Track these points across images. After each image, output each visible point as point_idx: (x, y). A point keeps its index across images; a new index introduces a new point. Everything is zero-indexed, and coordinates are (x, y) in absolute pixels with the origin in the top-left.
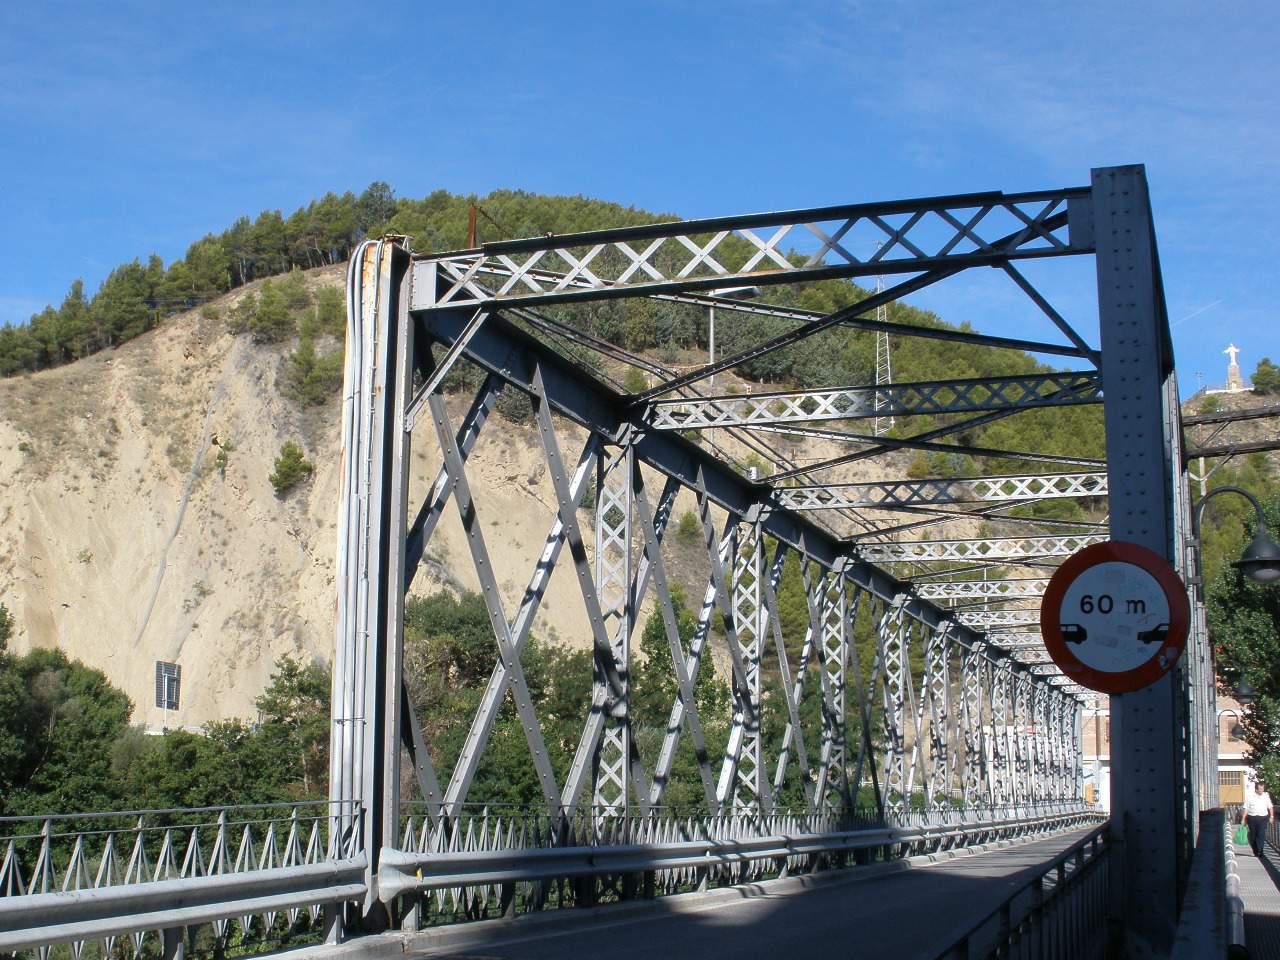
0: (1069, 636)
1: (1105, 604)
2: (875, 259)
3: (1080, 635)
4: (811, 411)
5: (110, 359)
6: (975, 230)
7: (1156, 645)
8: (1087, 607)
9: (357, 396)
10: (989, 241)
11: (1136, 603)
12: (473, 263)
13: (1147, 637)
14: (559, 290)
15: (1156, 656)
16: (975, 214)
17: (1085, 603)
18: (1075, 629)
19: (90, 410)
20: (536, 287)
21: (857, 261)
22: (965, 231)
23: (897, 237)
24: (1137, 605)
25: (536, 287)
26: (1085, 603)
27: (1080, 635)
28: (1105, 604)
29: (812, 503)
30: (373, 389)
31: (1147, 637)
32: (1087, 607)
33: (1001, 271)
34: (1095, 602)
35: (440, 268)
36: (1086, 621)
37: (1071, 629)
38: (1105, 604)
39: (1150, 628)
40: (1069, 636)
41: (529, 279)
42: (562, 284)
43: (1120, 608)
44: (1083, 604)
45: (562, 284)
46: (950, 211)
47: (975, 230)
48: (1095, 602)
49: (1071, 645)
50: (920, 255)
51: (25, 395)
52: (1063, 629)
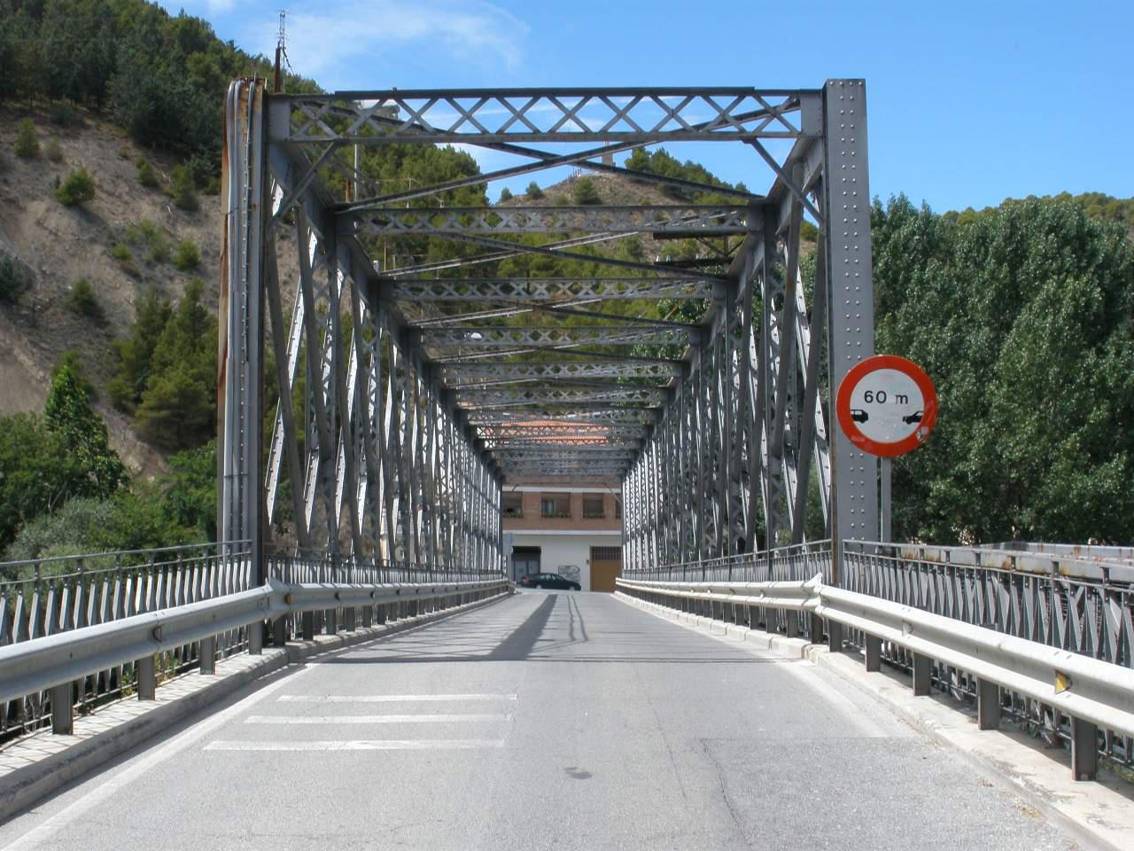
0: (856, 418)
1: (881, 397)
2: (655, 130)
3: (863, 417)
7: (915, 425)
8: (869, 399)
9: (236, 212)
10: (691, 123)
13: (909, 420)
15: (915, 433)
16: (667, 97)
18: (860, 413)
19: (1076, 307)
21: (642, 131)
22: (673, 114)
23: (519, 115)
24: (902, 398)
27: (863, 417)
28: (881, 397)
29: (450, 294)
30: (250, 206)
31: (909, 420)
32: (869, 399)
33: (750, 146)
36: (867, 408)
37: (857, 413)
38: (881, 397)
40: (856, 418)
43: (891, 399)
44: (866, 396)
46: (611, 99)
49: (857, 424)
50: (485, 132)
52: (852, 413)
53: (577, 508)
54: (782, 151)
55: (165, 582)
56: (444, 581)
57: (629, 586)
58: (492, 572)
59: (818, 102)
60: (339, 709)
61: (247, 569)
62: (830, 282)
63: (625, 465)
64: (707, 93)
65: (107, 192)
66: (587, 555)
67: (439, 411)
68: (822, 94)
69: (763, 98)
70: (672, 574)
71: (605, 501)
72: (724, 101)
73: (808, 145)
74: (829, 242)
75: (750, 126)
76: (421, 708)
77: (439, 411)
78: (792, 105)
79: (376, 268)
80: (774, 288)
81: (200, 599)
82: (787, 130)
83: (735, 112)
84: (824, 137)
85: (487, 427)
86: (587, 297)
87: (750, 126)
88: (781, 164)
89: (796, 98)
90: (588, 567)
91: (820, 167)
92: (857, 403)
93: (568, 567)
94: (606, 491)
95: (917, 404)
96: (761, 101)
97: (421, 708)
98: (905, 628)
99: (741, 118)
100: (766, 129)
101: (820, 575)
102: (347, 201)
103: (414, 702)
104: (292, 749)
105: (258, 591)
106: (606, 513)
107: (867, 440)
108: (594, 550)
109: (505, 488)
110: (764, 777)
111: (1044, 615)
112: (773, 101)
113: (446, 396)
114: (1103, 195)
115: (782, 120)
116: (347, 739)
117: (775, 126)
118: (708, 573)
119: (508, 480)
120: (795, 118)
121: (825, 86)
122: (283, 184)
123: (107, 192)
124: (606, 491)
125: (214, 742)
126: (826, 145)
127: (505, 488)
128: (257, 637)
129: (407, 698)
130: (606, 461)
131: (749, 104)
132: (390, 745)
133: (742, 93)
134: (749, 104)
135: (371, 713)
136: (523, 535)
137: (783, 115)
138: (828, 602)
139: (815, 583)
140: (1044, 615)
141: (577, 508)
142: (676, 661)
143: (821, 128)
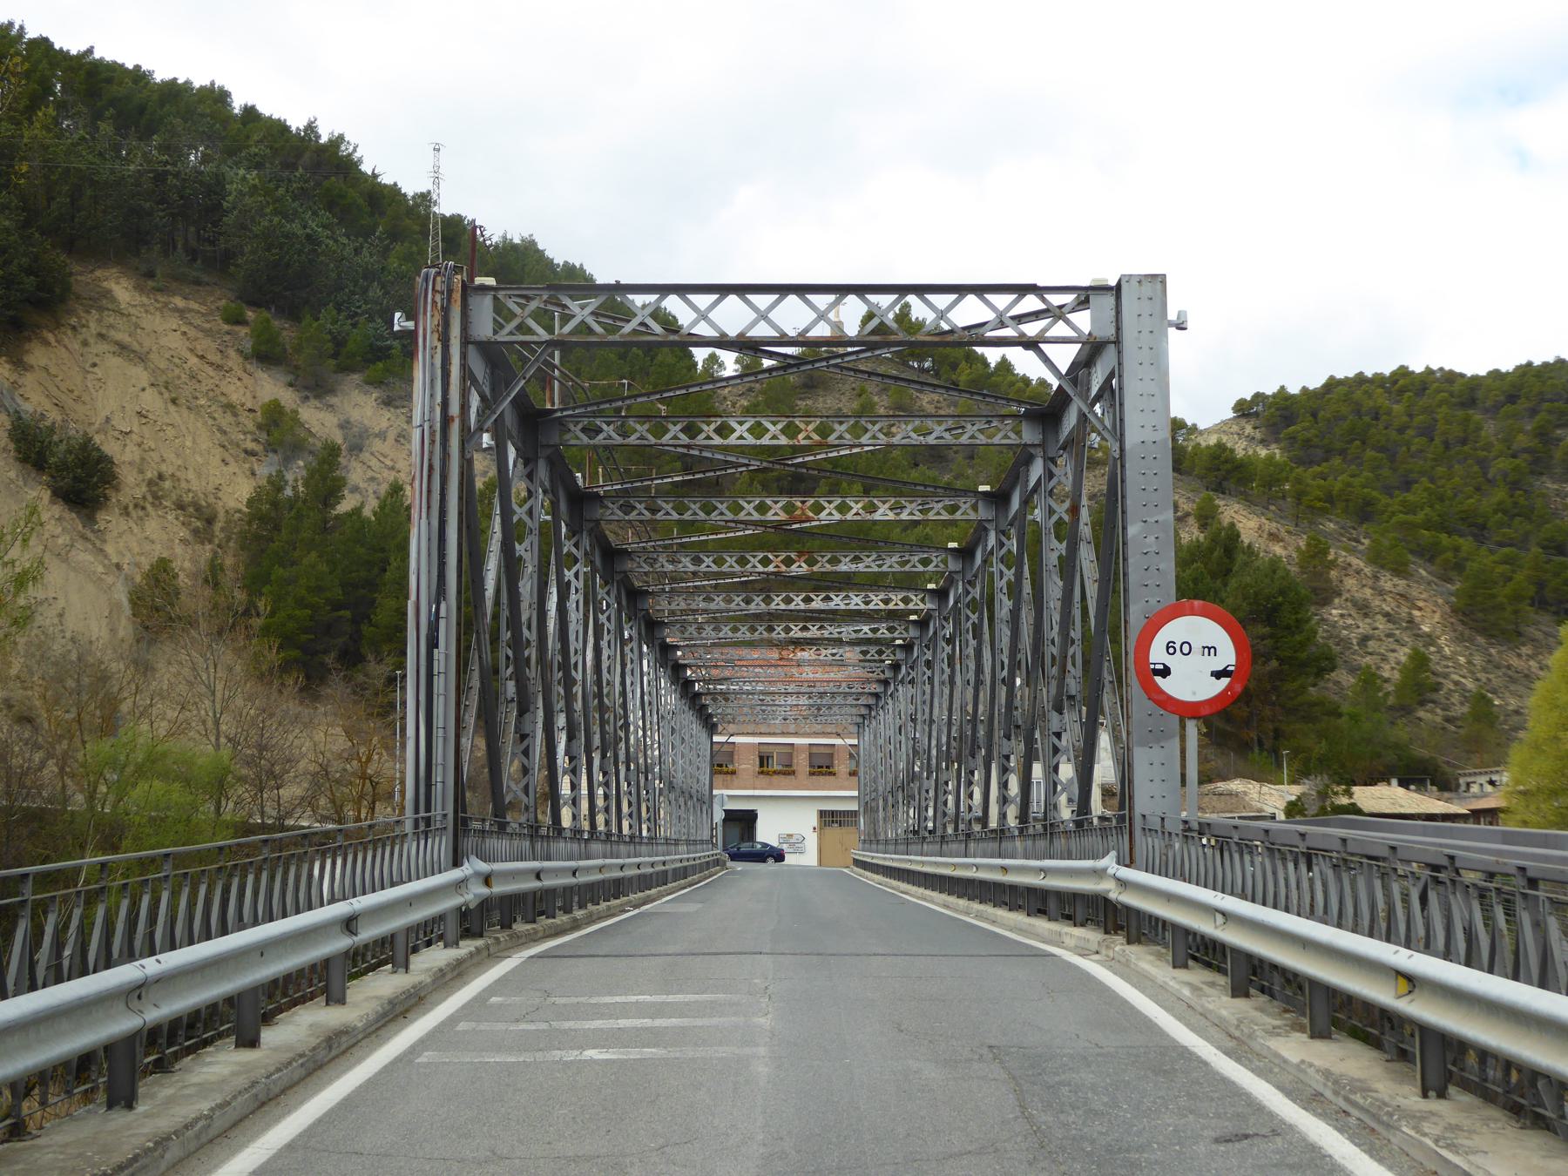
0: (1157, 672)
3: (1165, 672)
4: (725, 437)
5: (1392, 1028)
6: (754, 315)
7: (1225, 681)
8: (1171, 650)
11: (1209, 648)
12: (533, 299)
13: (1218, 675)
14: (622, 336)
17: (1170, 647)
18: (1161, 667)
20: (598, 329)
24: (1210, 650)
25: (598, 329)
26: (1170, 647)
27: (1165, 672)
28: (1186, 649)
31: (1218, 675)
32: (1171, 650)
33: (1031, 354)
34: (1177, 646)
35: (495, 298)
36: (1170, 661)
37: (1158, 667)
38: (1186, 649)
39: (1221, 668)
40: (1157, 672)
41: (591, 321)
42: (628, 328)
44: (1168, 648)
45: (628, 328)
47: (754, 315)
48: (1177, 646)
49: (1158, 679)
51: (34, 592)
53: (802, 763)
54: (1064, 356)
55: (374, 857)
56: (605, 857)
57: (869, 860)
58: (702, 842)
59: (1110, 300)
60: (564, 1013)
61: (441, 846)
62: (1123, 512)
63: (864, 711)
64: (980, 290)
65: (211, 364)
66: (814, 820)
67: (645, 648)
68: (1117, 290)
69: (1047, 296)
70: (925, 846)
71: (836, 757)
72: (1000, 301)
73: (1092, 350)
74: (1123, 466)
75: (1031, 329)
76: (659, 1011)
77: (645, 648)
78: (1083, 304)
79: (580, 482)
80: (1055, 512)
81: (393, 884)
82: (1074, 334)
83: (1015, 311)
84: (1117, 342)
85: (699, 667)
86: (829, 514)
87: (1031, 329)
88: (1064, 369)
89: (1085, 296)
90: (815, 835)
91: (1111, 375)
92: (1157, 655)
93: (790, 836)
94: (838, 741)
95: (1227, 656)
96: (1044, 300)
97: (659, 1011)
98: (1220, 918)
99: (1020, 319)
100: (1049, 334)
101: (1113, 854)
102: (548, 406)
103: (653, 1004)
104: (521, 1059)
105: (456, 874)
106: (836, 769)
107: (1170, 698)
108: (822, 814)
109: (716, 739)
110: (1065, 1090)
111: (1381, 905)
112: (1056, 300)
113: (651, 628)
114: (1403, 372)
115: (1068, 322)
116: (582, 1048)
117: (1060, 329)
118: (972, 845)
119: (720, 728)
120: (1083, 320)
121: (1120, 281)
122: (1238, 688)
123: (211, 364)
124: (838, 741)
125: (426, 1054)
126: (1119, 352)
127: (716, 739)
128: (451, 928)
129: (641, 998)
130: (841, 706)
131: (1031, 303)
132: (634, 1054)
133: (1022, 290)
134: (1031, 303)
135: (602, 1016)
136: (729, 796)
137: (1068, 316)
138: (1123, 884)
139: (1109, 862)
140: (1381, 905)
141: (802, 763)
142: (709, 954)
143: (1113, 331)
